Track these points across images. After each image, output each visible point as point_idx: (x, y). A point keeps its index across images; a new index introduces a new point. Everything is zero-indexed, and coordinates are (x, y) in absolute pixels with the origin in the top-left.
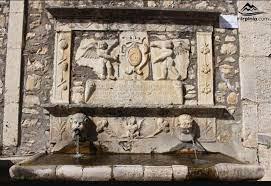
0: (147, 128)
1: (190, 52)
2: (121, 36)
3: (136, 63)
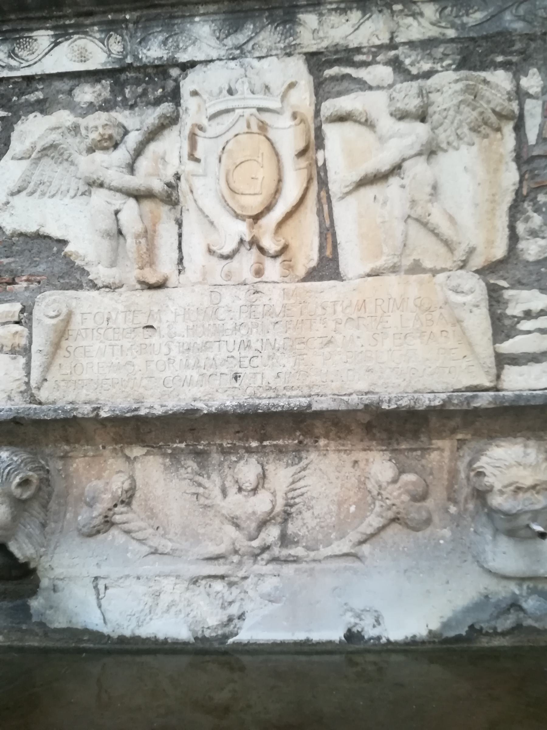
0: (321, 507)
1: (519, 128)
2: (187, 85)
3: (254, 204)
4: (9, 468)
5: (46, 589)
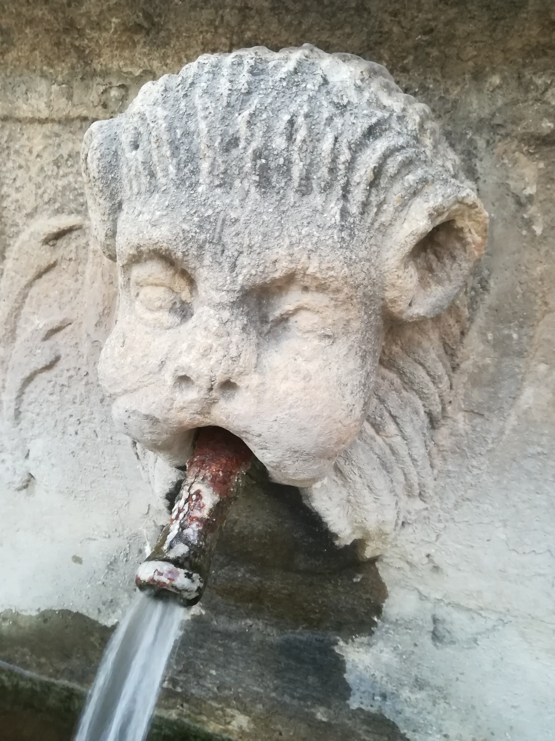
4: (380, 146)
5: (406, 625)
